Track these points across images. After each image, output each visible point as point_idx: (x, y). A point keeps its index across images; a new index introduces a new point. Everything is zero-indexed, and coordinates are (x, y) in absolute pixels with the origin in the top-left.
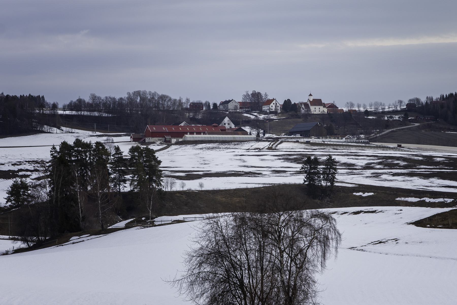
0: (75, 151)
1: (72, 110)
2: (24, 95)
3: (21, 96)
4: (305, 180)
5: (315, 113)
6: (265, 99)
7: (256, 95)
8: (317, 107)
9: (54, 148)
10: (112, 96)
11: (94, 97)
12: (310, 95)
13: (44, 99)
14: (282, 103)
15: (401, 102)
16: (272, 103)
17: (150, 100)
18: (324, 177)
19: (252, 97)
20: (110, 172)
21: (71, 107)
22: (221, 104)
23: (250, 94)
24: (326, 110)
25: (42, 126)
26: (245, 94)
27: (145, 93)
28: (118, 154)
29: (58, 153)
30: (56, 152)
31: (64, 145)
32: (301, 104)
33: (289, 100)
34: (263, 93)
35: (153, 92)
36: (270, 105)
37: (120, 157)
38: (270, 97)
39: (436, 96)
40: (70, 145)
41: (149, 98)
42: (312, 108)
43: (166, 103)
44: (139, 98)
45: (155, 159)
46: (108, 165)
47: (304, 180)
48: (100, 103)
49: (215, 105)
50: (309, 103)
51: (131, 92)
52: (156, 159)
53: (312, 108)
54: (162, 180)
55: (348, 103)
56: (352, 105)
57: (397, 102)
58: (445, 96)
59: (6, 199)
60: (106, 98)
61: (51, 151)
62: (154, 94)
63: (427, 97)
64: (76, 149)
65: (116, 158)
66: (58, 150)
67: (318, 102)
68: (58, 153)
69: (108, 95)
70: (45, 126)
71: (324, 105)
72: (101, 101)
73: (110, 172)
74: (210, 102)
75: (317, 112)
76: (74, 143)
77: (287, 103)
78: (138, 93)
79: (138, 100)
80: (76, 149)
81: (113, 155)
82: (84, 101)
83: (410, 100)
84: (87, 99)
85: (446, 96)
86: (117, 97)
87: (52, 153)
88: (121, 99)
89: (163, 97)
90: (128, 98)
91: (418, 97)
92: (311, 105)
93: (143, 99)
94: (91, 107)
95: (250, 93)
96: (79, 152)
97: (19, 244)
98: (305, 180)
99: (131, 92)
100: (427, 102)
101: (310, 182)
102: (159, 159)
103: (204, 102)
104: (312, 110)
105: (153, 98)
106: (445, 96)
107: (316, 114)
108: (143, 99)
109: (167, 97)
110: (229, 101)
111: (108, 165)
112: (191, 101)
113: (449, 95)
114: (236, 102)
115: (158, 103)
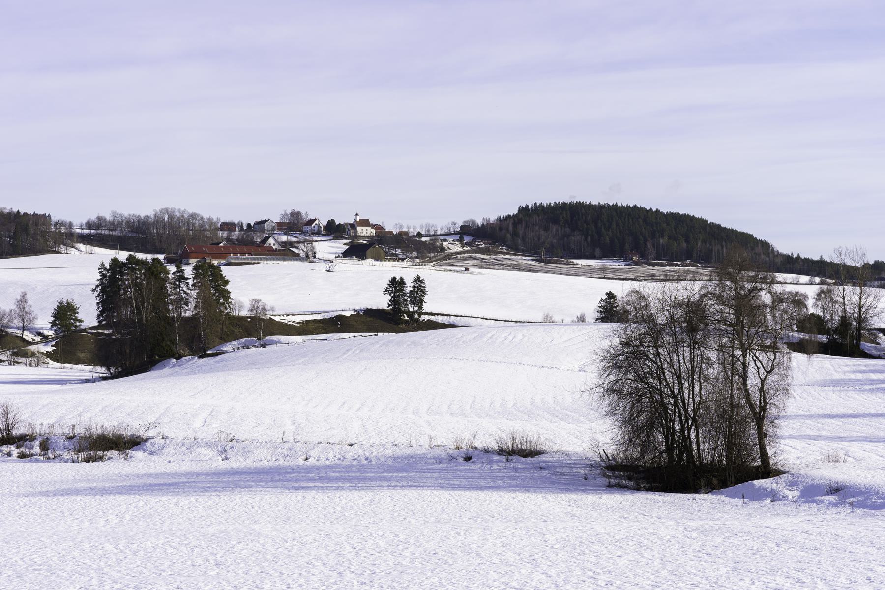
0: (128, 268)
1: (90, 228)
2: (559, 202)
3: (555, 203)
4: (390, 303)
5: (362, 235)
6: (306, 218)
7: (296, 215)
8: (365, 228)
9: (103, 265)
10: (137, 213)
11: (114, 215)
12: (357, 215)
13: (50, 218)
14: (325, 223)
15: (454, 224)
16: (314, 224)
17: (179, 219)
18: (411, 300)
19: (291, 216)
20: (169, 292)
21: (89, 225)
22: (255, 224)
23: (288, 213)
24: (373, 231)
25: (59, 247)
26: (283, 213)
27: (173, 211)
28: (179, 272)
29: (108, 271)
30: (105, 269)
31: (115, 261)
32: (347, 224)
33: (333, 220)
34: (303, 213)
35: (182, 209)
36: (311, 225)
37: (181, 276)
38: (311, 217)
39: (493, 218)
40: (122, 262)
41: (178, 216)
42: (359, 229)
43: (197, 222)
44: (167, 216)
45: (222, 277)
46: (168, 285)
47: (388, 304)
48: (122, 221)
49: (249, 225)
50: (355, 223)
51: (158, 209)
52: (224, 278)
53: (359, 229)
54: (230, 302)
55: (396, 224)
56: (401, 226)
57: (450, 223)
58: (502, 218)
59: (51, 323)
60: (130, 215)
61: (99, 269)
62: (184, 212)
63: (484, 219)
64: (129, 266)
65: (177, 276)
66: (108, 268)
67: (365, 223)
68: (108, 271)
69: (131, 213)
70: (62, 246)
71: (373, 226)
72: (124, 218)
73: (169, 292)
74: (243, 222)
75: (364, 234)
76: (127, 259)
77: (331, 223)
78: (166, 210)
79: (166, 219)
80: (129, 266)
81: (173, 274)
82: (105, 219)
83: (465, 222)
84: (109, 217)
85: (504, 217)
86: (142, 215)
87: (100, 271)
88: (147, 216)
89: (193, 216)
90: (155, 216)
91: (473, 219)
92: (130, 255)
93: (170, 217)
94: (113, 225)
95: (289, 212)
96: (133, 269)
97: (101, 370)
98: (390, 303)
99: (158, 211)
100: (483, 224)
101: (394, 306)
102: (226, 279)
103: (236, 222)
104: (359, 232)
105: (183, 216)
106: (502, 218)
107: (363, 236)
108: (170, 217)
109: (198, 215)
110: (266, 221)
111: (168, 285)
112: (222, 221)
113: (506, 217)
114: (273, 222)
115: (188, 222)
